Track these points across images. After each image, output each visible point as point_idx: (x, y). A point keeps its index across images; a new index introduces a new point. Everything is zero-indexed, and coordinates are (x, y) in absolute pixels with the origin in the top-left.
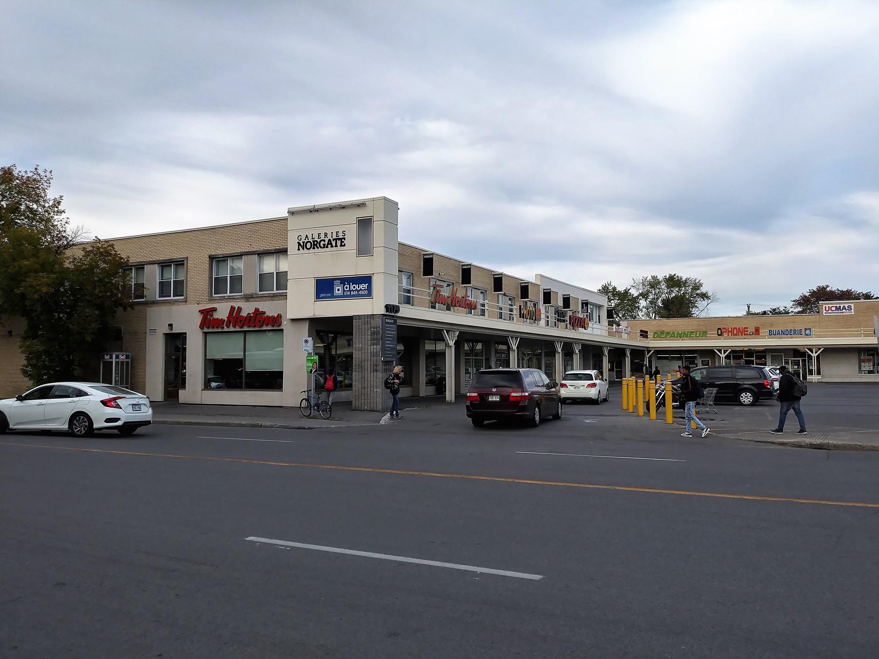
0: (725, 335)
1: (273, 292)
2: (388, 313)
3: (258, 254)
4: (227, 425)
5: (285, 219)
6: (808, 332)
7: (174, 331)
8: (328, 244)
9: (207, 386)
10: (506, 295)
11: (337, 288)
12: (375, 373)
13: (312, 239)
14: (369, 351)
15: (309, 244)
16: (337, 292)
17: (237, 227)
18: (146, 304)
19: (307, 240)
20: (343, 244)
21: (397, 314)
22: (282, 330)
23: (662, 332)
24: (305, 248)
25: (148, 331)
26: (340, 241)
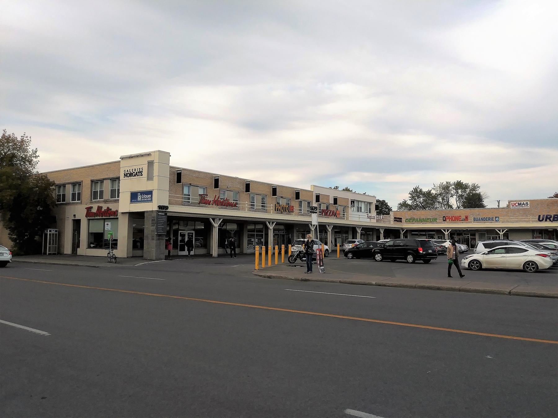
0: (448, 220)
1: (115, 199)
2: (160, 210)
3: (110, 179)
4: (26, 262)
5: (120, 162)
6: (497, 219)
8: (136, 174)
9: (89, 247)
10: (283, 197)
11: (139, 197)
12: (153, 241)
15: (128, 174)
16: (139, 199)
17: (80, 169)
18: (66, 204)
21: (167, 210)
22: (118, 218)
23: (414, 219)
25: (66, 218)
26: (140, 173)
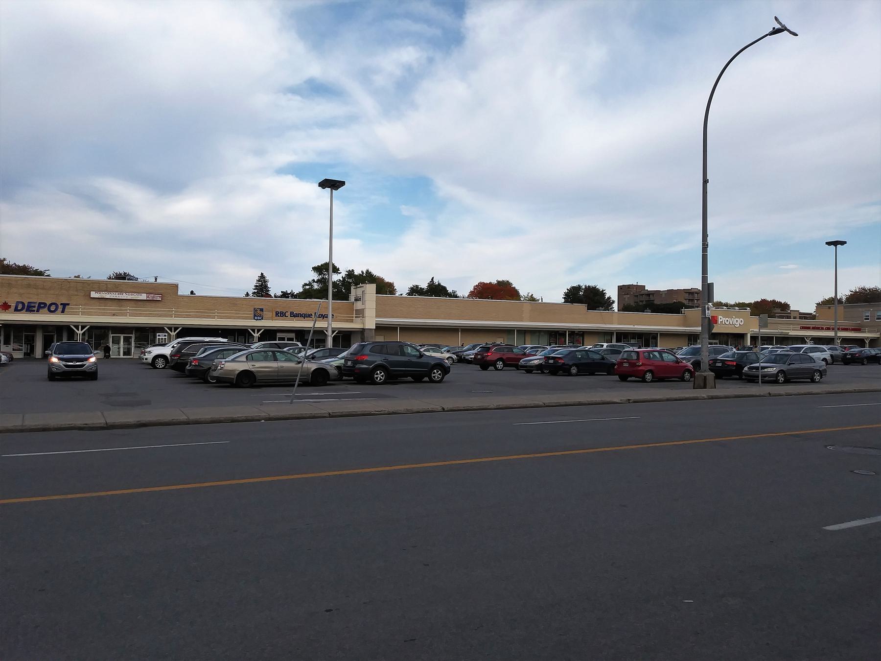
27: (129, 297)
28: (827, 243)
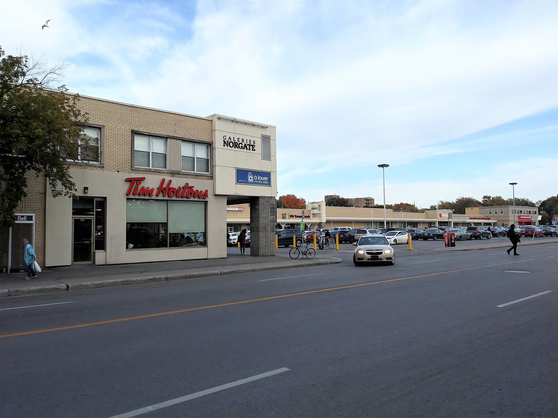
7: (88, 195)
8: (244, 147)
11: (250, 177)
13: (234, 141)
14: (270, 219)
16: (250, 180)
19: (230, 141)
20: (254, 149)
24: (229, 146)
27: (232, 209)
28: (510, 184)
